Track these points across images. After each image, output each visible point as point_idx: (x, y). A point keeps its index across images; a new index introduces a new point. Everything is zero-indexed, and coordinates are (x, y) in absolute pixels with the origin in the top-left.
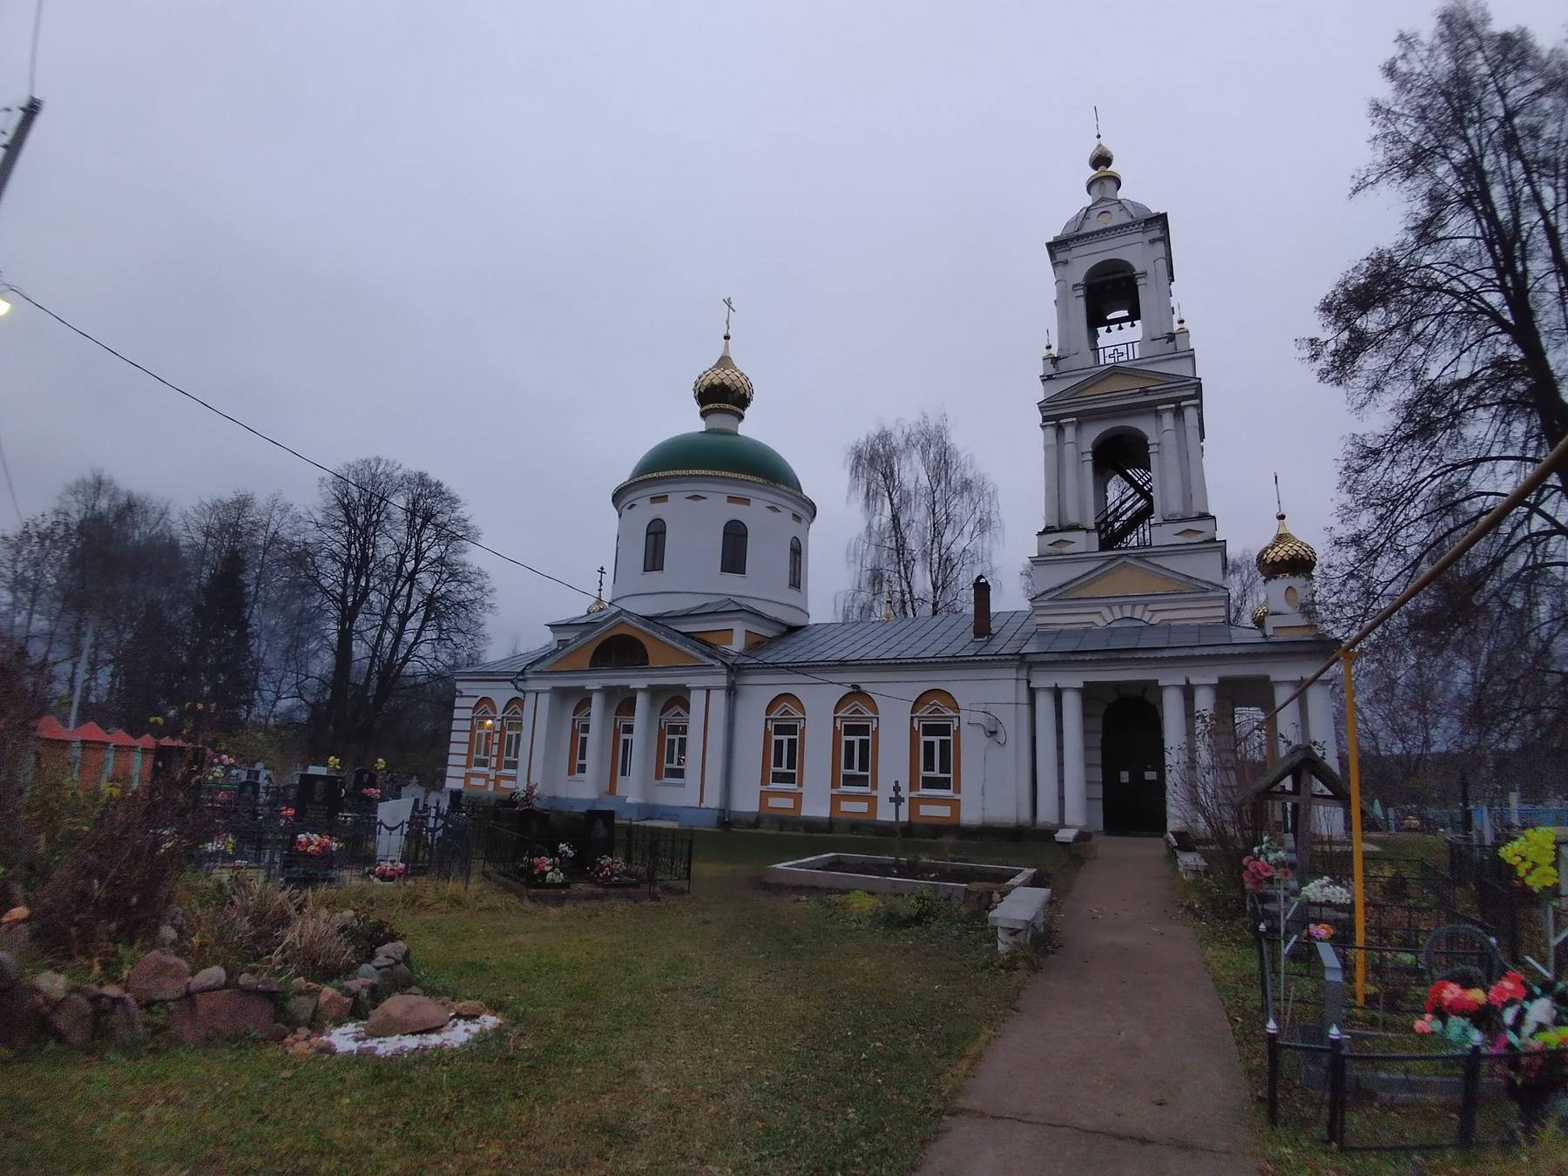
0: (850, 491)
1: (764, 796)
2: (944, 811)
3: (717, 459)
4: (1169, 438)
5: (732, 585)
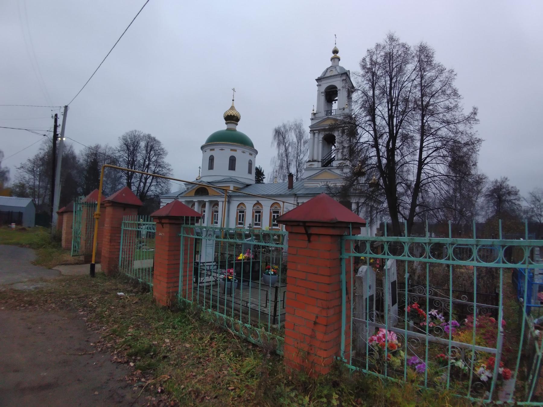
3: (230, 138)
5: (232, 174)
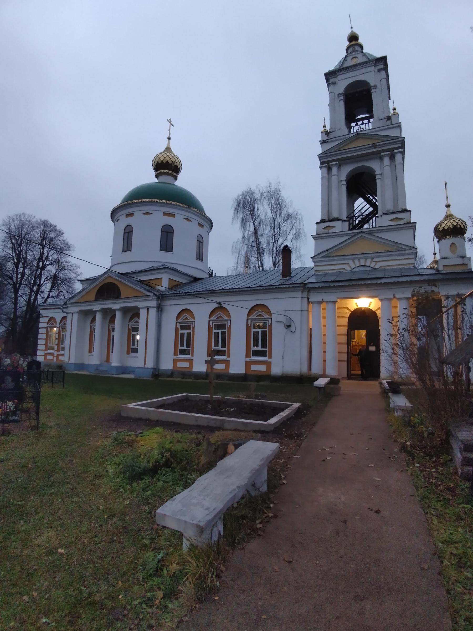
0: (234, 217)
1: (175, 361)
2: (263, 368)
3: (164, 193)
4: (387, 170)
